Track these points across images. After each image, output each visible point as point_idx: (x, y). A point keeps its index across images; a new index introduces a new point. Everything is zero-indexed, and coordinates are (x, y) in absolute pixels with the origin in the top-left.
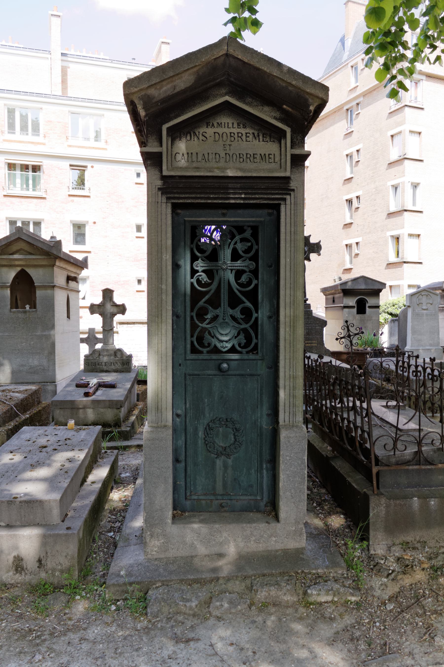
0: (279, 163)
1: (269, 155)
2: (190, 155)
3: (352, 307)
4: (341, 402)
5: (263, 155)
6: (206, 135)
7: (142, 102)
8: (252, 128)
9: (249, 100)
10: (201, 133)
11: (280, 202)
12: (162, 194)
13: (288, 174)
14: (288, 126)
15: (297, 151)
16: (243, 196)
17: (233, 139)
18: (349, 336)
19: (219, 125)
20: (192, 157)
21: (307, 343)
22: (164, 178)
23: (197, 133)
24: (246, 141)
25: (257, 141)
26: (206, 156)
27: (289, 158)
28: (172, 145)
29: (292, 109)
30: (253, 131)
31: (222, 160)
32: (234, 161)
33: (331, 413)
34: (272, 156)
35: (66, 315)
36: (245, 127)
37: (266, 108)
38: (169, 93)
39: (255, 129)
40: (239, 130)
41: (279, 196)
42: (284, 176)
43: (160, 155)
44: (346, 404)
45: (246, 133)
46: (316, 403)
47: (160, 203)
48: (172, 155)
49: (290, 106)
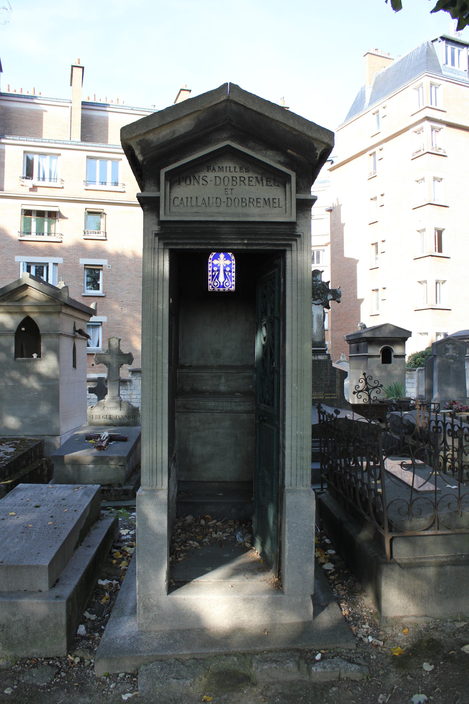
0: (284, 207)
1: (273, 199)
2: (189, 199)
3: (379, 356)
4: (356, 462)
5: (266, 199)
6: (207, 179)
7: (139, 147)
8: (255, 172)
9: (252, 144)
10: (201, 177)
11: (285, 248)
12: (159, 239)
13: (293, 219)
14: (293, 170)
15: (302, 196)
16: (246, 242)
17: (235, 183)
18: (367, 389)
19: (221, 169)
20: (191, 201)
21: (327, 396)
22: (161, 223)
23: (197, 178)
24: (249, 185)
25: (261, 185)
26: (207, 200)
27: (294, 202)
28: (170, 190)
29: (298, 153)
30: (256, 175)
31: (224, 205)
32: (236, 205)
33: (346, 473)
34: (276, 201)
35: (72, 364)
36: (247, 171)
37: (270, 153)
38: (169, 137)
39: (258, 173)
40: (241, 174)
41: (285, 242)
42: (289, 221)
43: (157, 199)
44: (360, 463)
45: (249, 177)
46: (331, 462)
47: (156, 250)
48: (170, 199)
49: (296, 151)
